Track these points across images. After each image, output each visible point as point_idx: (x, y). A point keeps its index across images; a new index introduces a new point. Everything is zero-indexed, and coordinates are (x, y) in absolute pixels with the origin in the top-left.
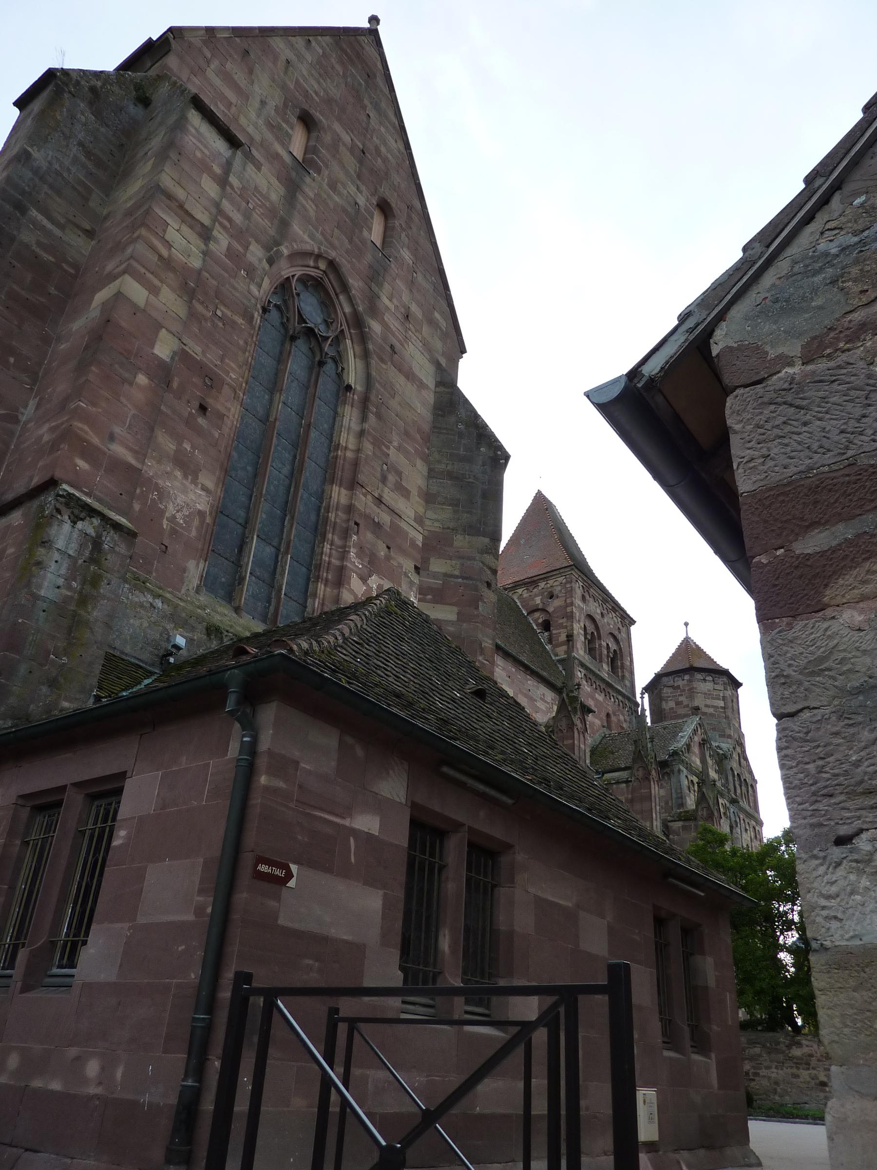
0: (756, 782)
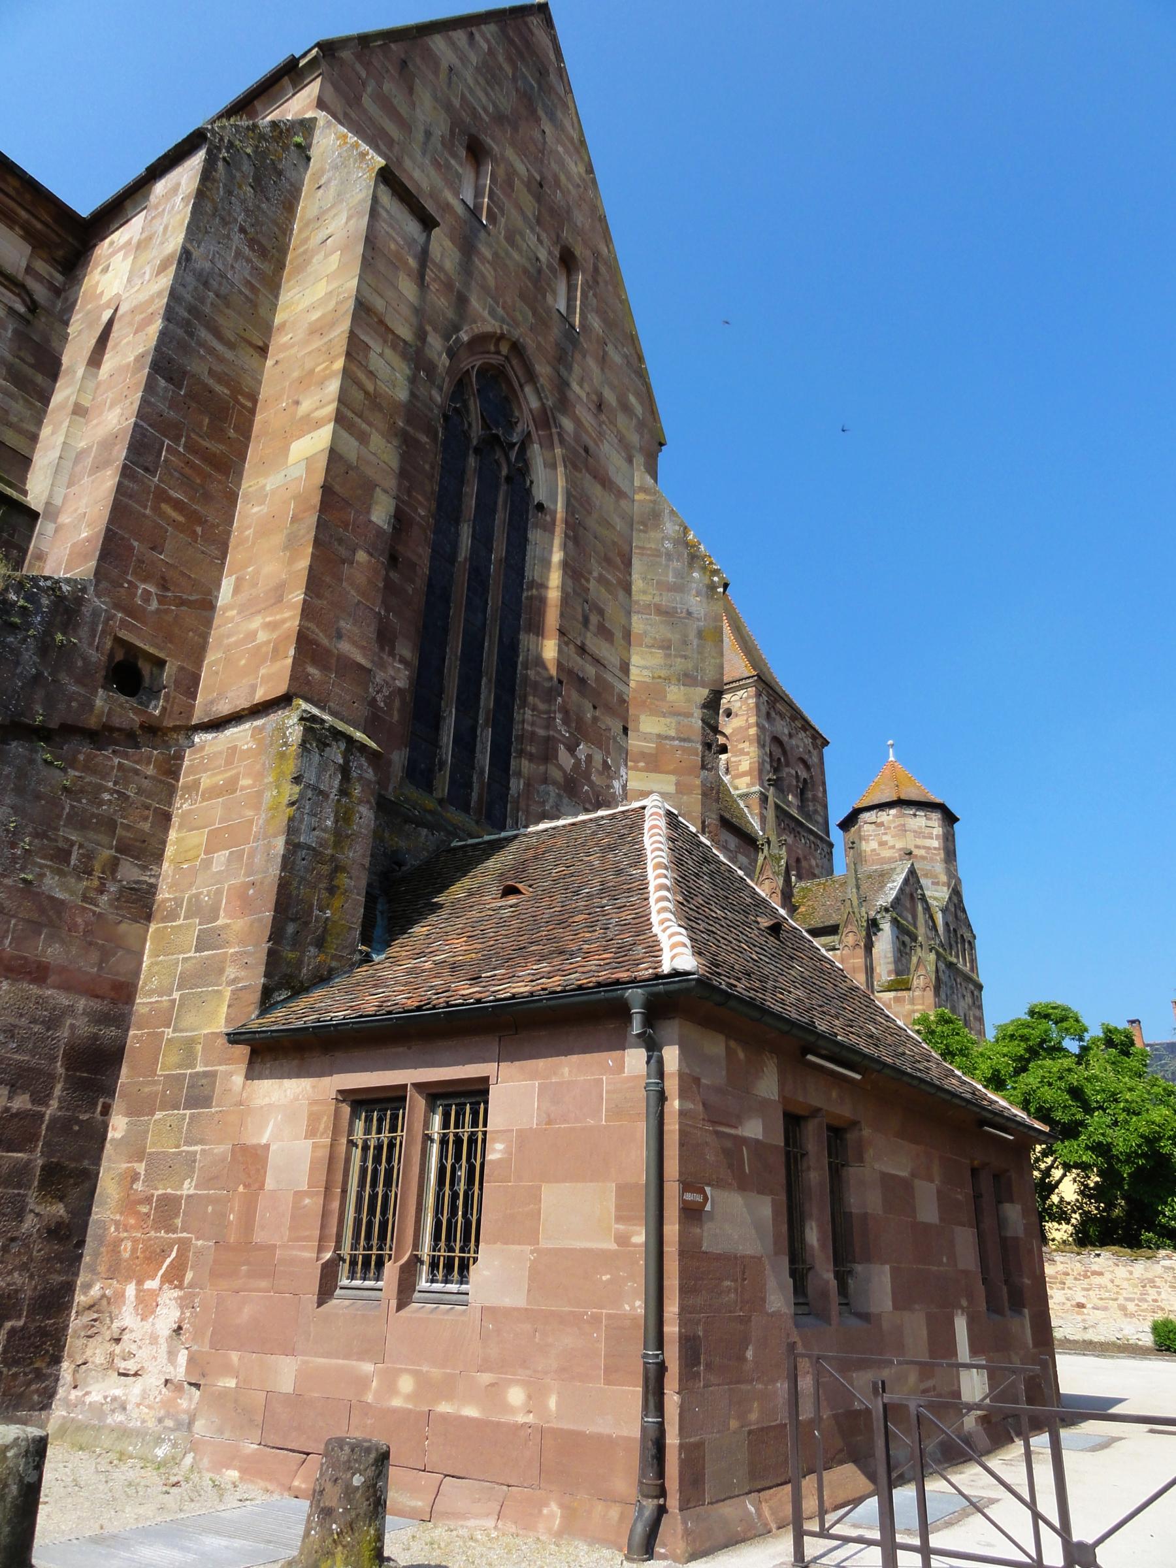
0: (974, 937)
